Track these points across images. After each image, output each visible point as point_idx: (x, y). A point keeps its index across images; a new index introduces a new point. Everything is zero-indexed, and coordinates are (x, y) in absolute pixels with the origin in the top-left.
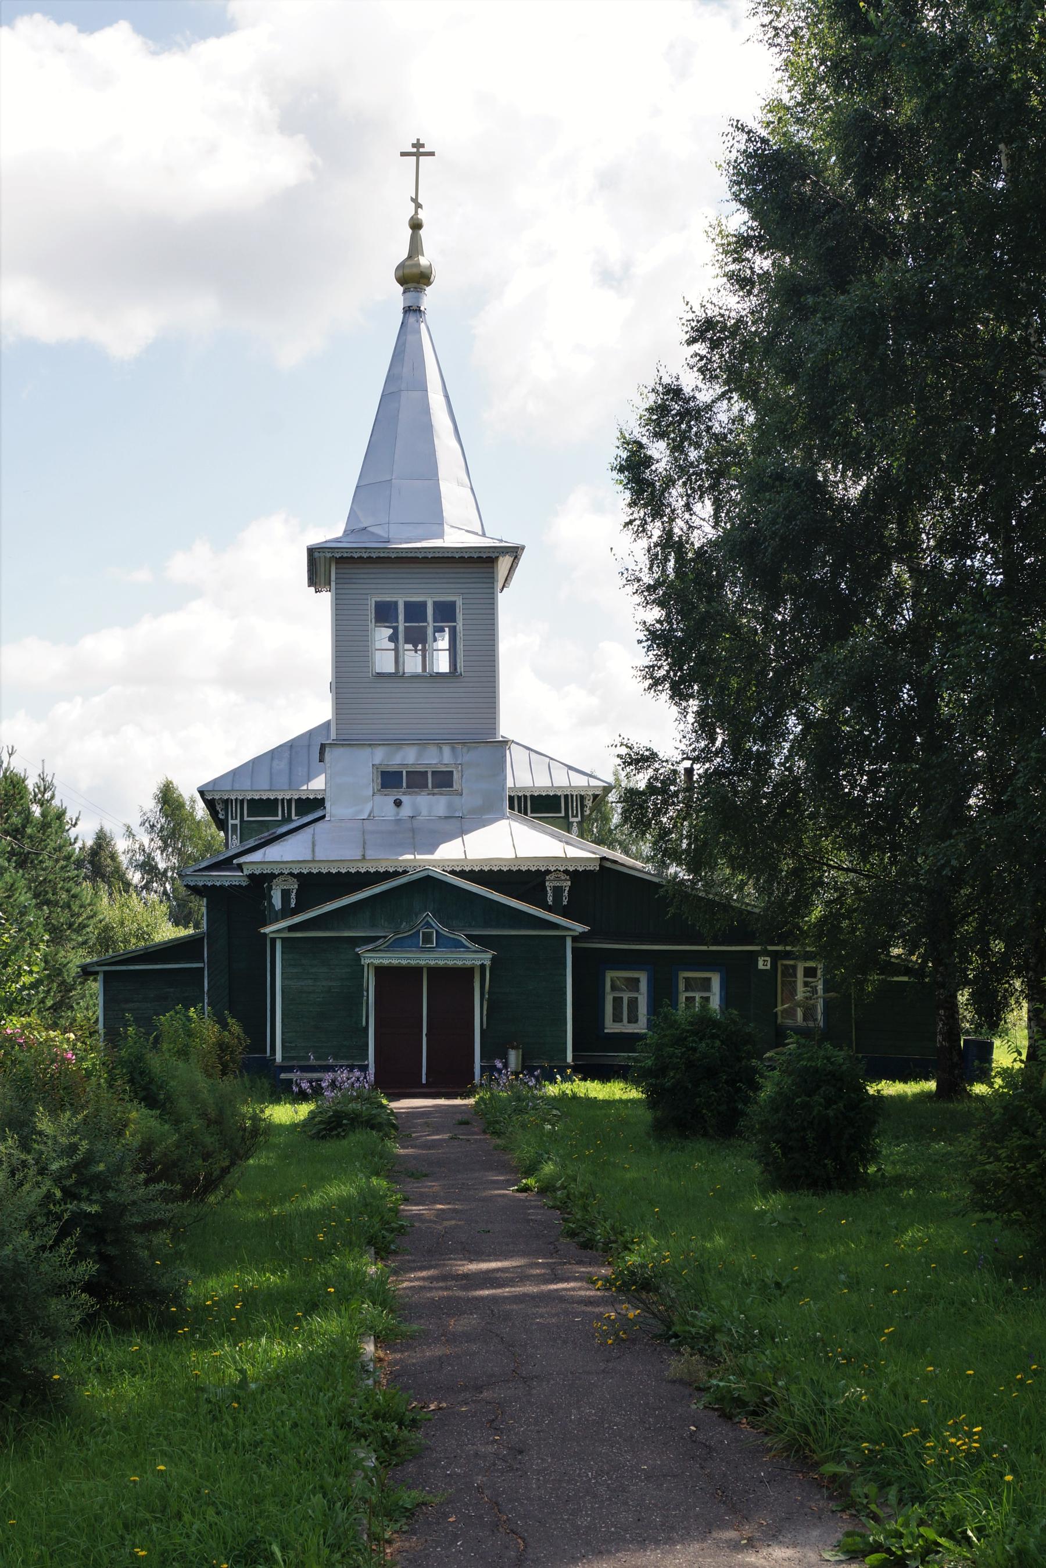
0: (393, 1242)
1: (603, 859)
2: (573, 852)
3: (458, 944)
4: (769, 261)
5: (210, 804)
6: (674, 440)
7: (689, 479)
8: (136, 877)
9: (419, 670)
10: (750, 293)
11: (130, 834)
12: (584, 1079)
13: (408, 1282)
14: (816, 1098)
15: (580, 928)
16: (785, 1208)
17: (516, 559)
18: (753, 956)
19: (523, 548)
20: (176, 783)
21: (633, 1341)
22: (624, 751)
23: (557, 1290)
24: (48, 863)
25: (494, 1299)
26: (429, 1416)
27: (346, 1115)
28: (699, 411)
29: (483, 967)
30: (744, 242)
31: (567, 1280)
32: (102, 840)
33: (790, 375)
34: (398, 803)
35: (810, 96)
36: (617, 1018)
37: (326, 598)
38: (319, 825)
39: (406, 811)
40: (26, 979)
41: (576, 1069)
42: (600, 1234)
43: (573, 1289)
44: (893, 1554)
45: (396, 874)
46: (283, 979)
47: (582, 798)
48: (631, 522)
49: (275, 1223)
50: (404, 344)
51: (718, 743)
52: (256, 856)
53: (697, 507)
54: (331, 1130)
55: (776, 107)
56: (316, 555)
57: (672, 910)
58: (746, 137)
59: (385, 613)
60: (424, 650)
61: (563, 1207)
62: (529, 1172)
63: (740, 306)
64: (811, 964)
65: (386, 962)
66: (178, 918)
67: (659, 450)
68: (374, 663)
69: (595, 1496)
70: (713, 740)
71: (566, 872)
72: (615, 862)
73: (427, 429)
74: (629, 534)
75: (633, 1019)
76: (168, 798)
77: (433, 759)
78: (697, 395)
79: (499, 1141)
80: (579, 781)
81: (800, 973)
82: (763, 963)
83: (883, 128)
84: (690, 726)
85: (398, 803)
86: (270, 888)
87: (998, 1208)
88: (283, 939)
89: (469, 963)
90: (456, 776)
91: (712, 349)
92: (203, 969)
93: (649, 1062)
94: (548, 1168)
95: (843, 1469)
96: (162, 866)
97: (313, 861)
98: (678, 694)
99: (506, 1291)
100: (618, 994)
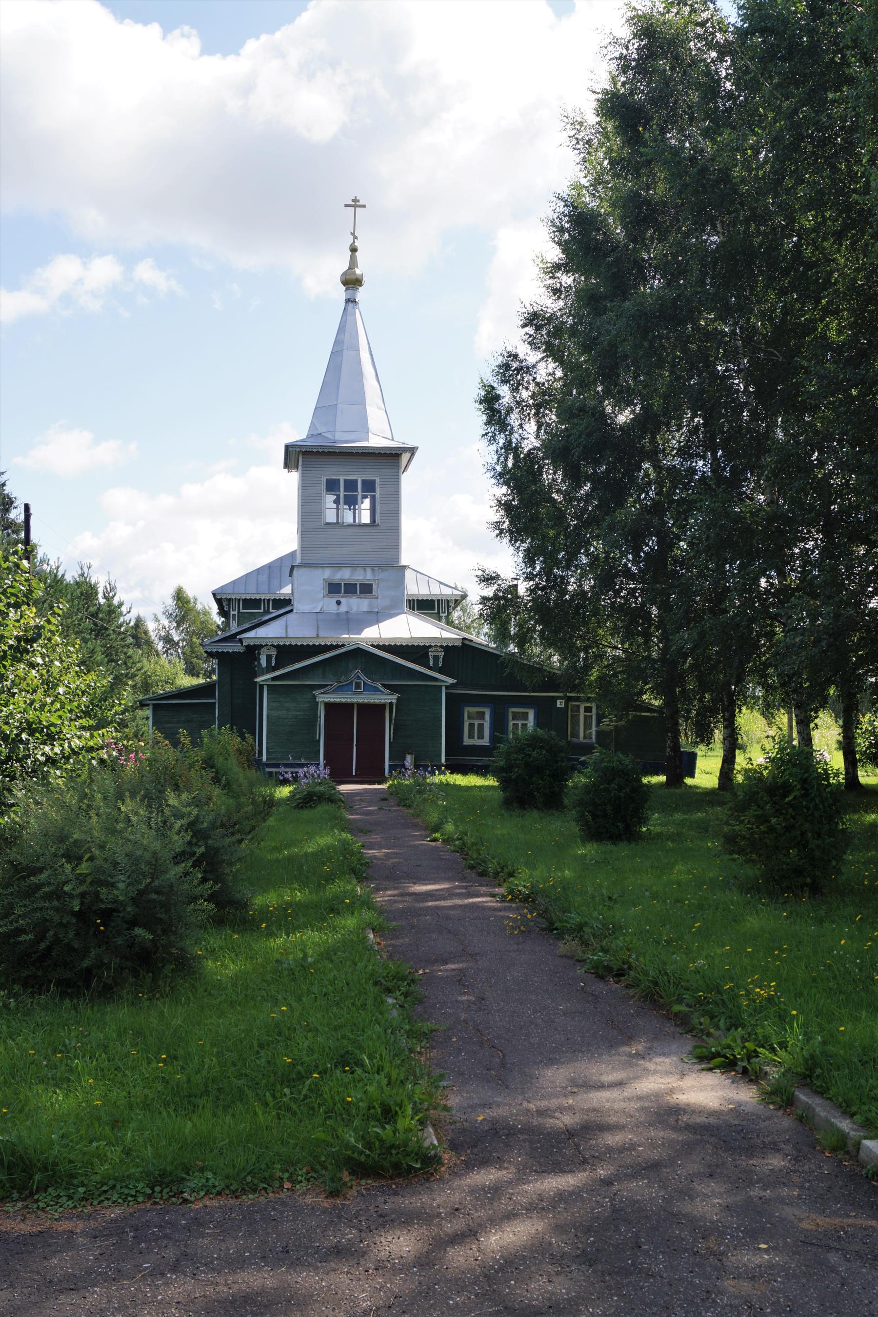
0: (364, 872)
1: (464, 639)
2: (446, 635)
3: (378, 690)
4: (572, 278)
5: (219, 602)
6: (513, 385)
7: (522, 409)
8: (160, 646)
9: (351, 521)
10: (559, 298)
11: (157, 620)
12: (452, 773)
13: (380, 898)
14: (612, 786)
15: (451, 681)
16: (596, 852)
17: (413, 454)
18: (554, 699)
19: (417, 448)
20: (184, 588)
21: (529, 932)
22: (480, 573)
23: (480, 902)
24: (113, 636)
25: (437, 907)
26: (421, 977)
27: (315, 794)
28: (528, 368)
29: (391, 704)
30: (557, 267)
31: (477, 896)
32: (139, 622)
33: (586, 348)
34: (339, 603)
35: (597, 182)
36: (471, 736)
37: (294, 477)
38: (290, 615)
39: (343, 608)
40: (118, 708)
41: (447, 767)
42: (491, 867)
43: (486, 902)
44: (727, 1058)
45: (337, 647)
46: (268, 710)
47: (448, 601)
48: (486, 434)
49: (290, 859)
50: (345, 322)
51: (538, 568)
52: (251, 634)
53: (526, 426)
54: (307, 803)
55: (577, 187)
56: (290, 449)
57: (508, 670)
58: (563, 204)
59: (332, 486)
60: (355, 509)
61: (461, 850)
62: (436, 829)
63: (553, 306)
64: (588, 705)
65: (332, 700)
66: (191, 671)
67: (504, 391)
68: (325, 517)
69: (536, 1025)
70: (534, 568)
71: (441, 646)
72: (471, 641)
73: (359, 374)
74: (485, 442)
75: (481, 736)
76: (180, 597)
77: (360, 577)
78: (527, 358)
79: (412, 811)
80: (447, 591)
81: (582, 710)
82: (560, 704)
83: (648, 202)
84: (521, 559)
85: (339, 603)
86: (259, 654)
87: (741, 852)
88: (268, 685)
89: (383, 701)
90: (374, 587)
91: (537, 330)
92: (215, 703)
93: (502, 763)
94: (450, 827)
95: (683, 1008)
96: (176, 638)
97: (287, 637)
98: (513, 540)
99: (442, 903)
100: (472, 721)
